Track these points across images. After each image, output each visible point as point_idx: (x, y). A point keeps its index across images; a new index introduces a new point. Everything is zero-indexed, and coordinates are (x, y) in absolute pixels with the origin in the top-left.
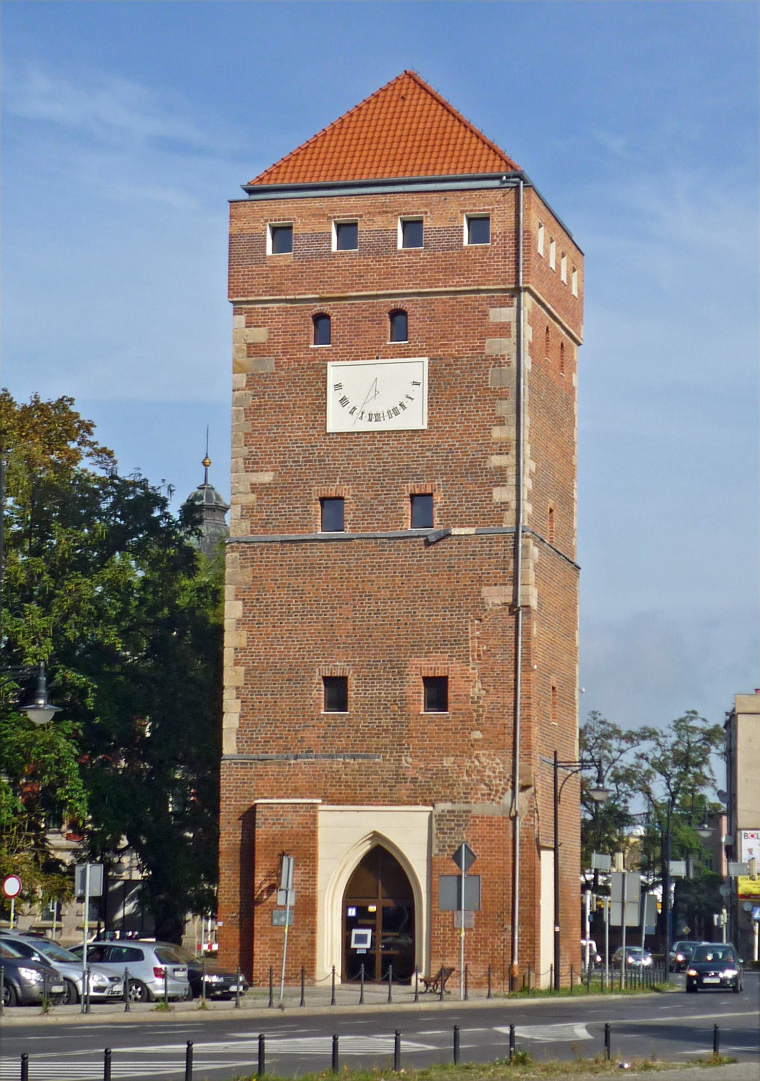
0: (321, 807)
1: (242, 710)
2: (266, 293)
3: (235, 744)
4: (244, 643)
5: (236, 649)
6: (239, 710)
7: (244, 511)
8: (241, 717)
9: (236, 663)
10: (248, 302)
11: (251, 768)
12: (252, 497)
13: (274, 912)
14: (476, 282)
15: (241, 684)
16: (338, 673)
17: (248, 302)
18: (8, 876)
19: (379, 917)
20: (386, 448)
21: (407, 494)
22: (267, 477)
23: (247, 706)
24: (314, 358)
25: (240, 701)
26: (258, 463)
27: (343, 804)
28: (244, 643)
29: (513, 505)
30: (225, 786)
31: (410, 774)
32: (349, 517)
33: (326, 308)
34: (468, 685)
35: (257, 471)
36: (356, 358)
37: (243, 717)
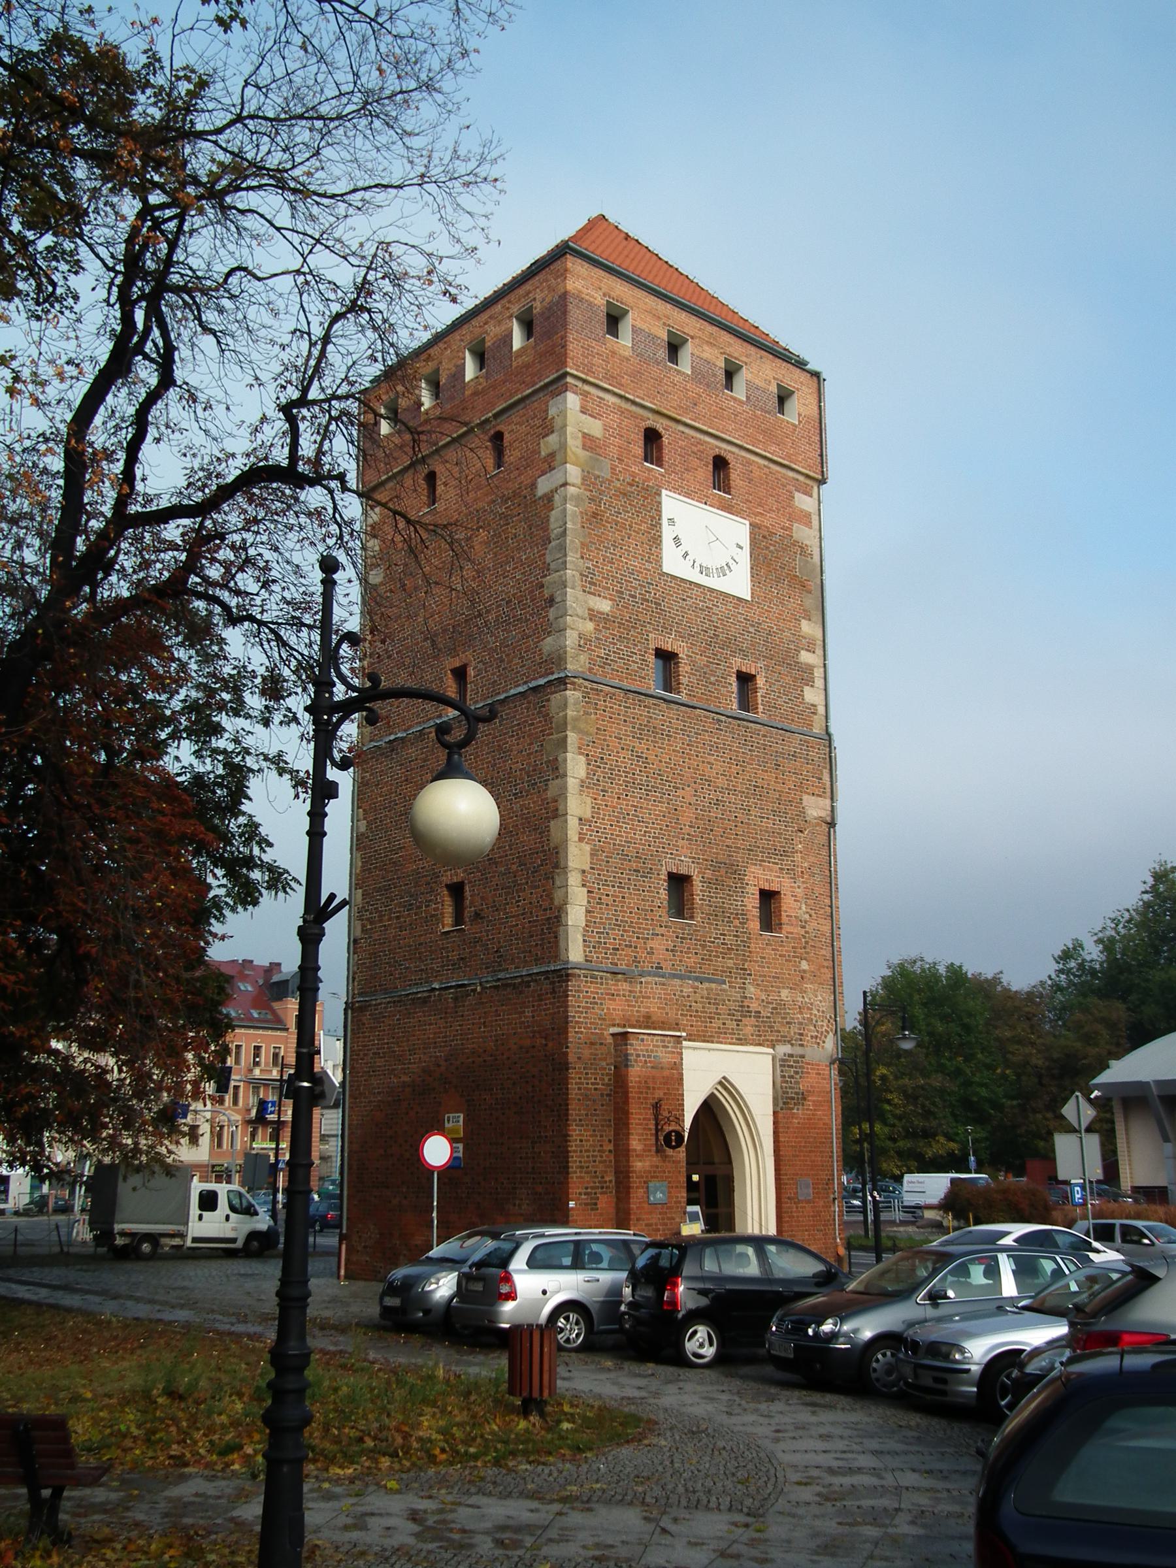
0: (685, 1043)
1: (589, 902)
2: (605, 379)
3: (581, 948)
4: (588, 815)
5: (581, 819)
6: (585, 903)
7: (582, 642)
8: (588, 911)
9: (581, 840)
10: (585, 381)
11: (602, 984)
12: (590, 626)
13: (651, 1185)
14: (788, 456)
15: (587, 867)
16: (683, 871)
17: (585, 381)
18: (441, 1131)
19: (702, 1187)
20: (715, 610)
21: (735, 670)
22: (605, 606)
23: (594, 898)
24: (649, 479)
25: (585, 890)
26: (595, 584)
27: (694, 1041)
28: (588, 815)
29: (821, 710)
30: (573, 1006)
31: (754, 1006)
32: (684, 680)
33: (660, 424)
34: (792, 906)
35: (594, 594)
36: (688, 495)
37: (589, 912)
